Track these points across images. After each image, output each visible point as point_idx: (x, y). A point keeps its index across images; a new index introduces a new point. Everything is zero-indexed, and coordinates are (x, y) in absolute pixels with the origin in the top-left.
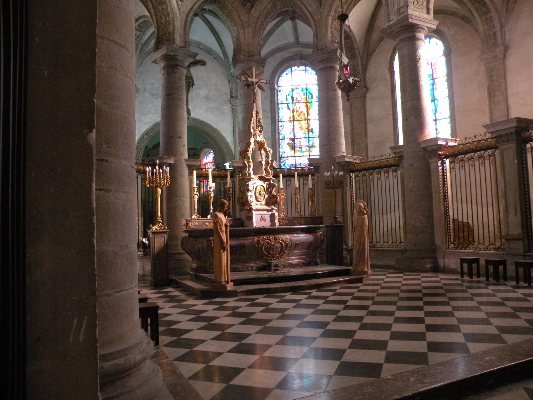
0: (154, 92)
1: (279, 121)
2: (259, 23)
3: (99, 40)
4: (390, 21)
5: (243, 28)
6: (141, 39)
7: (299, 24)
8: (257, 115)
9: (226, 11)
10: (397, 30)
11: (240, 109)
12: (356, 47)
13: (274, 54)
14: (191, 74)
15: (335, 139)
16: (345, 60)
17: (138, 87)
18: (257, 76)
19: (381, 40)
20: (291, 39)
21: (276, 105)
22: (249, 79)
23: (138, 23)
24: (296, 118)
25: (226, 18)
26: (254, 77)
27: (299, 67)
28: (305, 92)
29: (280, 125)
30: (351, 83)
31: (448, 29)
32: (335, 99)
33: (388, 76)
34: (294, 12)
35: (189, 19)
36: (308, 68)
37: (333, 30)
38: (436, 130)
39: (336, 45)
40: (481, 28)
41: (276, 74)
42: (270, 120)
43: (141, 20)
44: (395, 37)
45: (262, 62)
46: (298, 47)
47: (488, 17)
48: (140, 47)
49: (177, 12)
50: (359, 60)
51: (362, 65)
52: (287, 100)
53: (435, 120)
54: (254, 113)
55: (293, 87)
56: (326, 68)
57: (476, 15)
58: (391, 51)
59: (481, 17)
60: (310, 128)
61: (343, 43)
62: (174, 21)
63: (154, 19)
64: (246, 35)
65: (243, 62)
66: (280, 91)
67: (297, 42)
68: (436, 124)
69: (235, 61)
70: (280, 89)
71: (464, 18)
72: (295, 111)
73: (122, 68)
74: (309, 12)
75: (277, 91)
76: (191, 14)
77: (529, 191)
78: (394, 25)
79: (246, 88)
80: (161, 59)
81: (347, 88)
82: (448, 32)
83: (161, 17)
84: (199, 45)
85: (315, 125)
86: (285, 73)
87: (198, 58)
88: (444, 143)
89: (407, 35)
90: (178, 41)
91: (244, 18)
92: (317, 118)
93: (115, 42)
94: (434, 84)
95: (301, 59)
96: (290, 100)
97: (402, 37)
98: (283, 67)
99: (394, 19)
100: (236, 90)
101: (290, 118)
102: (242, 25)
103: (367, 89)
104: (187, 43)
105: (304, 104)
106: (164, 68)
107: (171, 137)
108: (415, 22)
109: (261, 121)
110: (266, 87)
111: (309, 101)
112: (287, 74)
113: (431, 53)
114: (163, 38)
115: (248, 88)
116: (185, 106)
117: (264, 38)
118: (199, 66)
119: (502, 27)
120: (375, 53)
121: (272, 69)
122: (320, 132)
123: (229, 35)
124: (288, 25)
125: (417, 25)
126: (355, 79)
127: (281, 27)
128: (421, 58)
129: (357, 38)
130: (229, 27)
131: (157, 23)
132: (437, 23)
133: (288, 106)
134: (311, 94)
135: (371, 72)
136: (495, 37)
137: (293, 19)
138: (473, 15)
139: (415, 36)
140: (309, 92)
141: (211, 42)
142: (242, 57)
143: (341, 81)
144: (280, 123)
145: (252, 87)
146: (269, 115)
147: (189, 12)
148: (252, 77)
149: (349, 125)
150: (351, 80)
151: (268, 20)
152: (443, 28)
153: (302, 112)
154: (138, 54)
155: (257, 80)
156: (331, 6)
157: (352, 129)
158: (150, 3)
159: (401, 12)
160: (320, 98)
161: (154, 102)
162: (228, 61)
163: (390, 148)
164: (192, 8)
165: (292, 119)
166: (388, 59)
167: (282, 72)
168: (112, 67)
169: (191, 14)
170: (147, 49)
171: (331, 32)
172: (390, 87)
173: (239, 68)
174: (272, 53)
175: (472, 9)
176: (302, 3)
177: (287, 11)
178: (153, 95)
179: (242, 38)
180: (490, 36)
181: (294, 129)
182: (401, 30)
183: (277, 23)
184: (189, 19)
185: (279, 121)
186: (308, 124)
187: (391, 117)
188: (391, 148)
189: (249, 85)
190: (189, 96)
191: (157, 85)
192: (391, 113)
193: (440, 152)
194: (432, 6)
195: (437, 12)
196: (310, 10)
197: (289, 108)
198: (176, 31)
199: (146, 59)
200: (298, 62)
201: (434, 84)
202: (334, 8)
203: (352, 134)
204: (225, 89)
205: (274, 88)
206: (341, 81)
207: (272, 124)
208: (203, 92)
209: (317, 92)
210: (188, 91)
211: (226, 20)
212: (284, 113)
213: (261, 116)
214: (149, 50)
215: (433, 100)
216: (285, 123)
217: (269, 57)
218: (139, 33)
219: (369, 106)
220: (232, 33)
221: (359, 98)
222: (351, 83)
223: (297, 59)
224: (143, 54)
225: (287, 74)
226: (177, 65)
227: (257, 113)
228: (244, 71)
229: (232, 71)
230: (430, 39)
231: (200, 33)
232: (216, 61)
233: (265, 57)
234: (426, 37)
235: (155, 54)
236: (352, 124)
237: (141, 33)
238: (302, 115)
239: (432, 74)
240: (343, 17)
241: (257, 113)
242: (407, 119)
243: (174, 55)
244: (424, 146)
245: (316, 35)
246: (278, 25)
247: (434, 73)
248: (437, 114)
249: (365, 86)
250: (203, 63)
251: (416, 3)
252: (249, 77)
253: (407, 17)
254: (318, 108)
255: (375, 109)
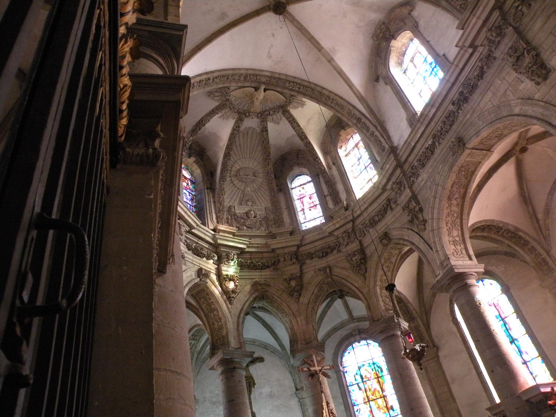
0: (214, 400)
1: (354, 405)
2: (310, 309)
3: (155, 372)
4: (437, 276)
5: (295, 318)
6: (196, 347)
7: (349, 300)
8: (328, 407)
9: (275, 304)
10: (447, 283)
11: (308, 402)
12: (412, 308)
13: (332, 335)
14: (250, 373)
15: (421, 413)
16: (405, 325)
17: (197, 398)
18: (319, 363)
19: (434, 295)
20: (345, 316)
21: (346, 388)
22: (312, 369)
23: (192, 333)
24: (371, 397)
25: (276, 312)
26: (316, 365)
27: (359, 342)
28: (373, 367)
29: (355, 410)
30: (419, 350)
31: (496, 267)
32: (408, 368)
33: (455, 329)
34: (341, 291)
35: (241, 320)
36: (369, 341)
37: (384, 298)
38: (532, 374)
39: (392, 312)
40: (528, 258)
41: (338, 355)
42: (343, 406)
43: (195, 329)
44: (447, 291)
45: (321, 347)
46: (354, 322)
47: (529, 247)
48: (196, 355)
49: (229, 315)
50: (419, 320)
51: (424, 325)
52: (356, 380)
53: (525, 363)
54: (324, 404)
55: (359, 365)
56: (387, 337)
57: (517, 248)
58: (449, 303)
59: (523, 250)
60: (389, 405)
61: (398, 308)
62: (226, 324)
63: (207, 326)
64: (300, 323)
65: (301, 351)
66: (346, 372)
67: (352, 318)
68: (528, 367)
69: (293, 351)
70: (346, 369)
71: (506, 254)
72: (368, 390)
73: (181, 397)
74: (356, 287)
75: (344, 373)
76: (242, 315)
77: (483, 187)
78: (442, 279)
79: (310, 378)
80: (218, 365)
81: (417, 357)
82: (498, 270)
83: (213, 324)
84: (253, 342)
85: (393, 400)
86: (347, 352)
87: (255, 355)
88: (548, 390)
89: (458, 286)
90: (233, 343)
91: (294, 307)
92: (394, 392)
93: (171, 371)
94: (505, 324)
95: (361, 334)
96: (359, 380)
97: (455, 287)
98: (344, 347)
99: (440, 273)
100: (300, 381)
101: (364, 399)
102: (294, 315)
103: (436, 348)
104: (242, 343)
105: (376, 380)
106: (222, 373)
107: (233, 400)
108: (461, 271)
109: (334, 411)
110: (330, 373)
111: (380, 375)
112: (349, 353)
113: (489, 294)
114: (218, 343)
115: (312, 378)
116: (250, 411)
117: (318, 321)
118: (258, 364)
119: (548, 253)
120: (433, 309)
121: (333, 351)
122: (400, 408)
123: (283, 327)
124: (338, 304)
125: (464, 273)
126: (422, 345)
127: (332, 307)
128: (481, 303)
129: (410, 300)
130: (281, 319)
131: (210, 330)
132: (483, 266)
133: (359, 386)
134: (379, 367)
135: (435, 329)
136: (547, 263)
137: (341, 297)
138: (514, 249)
139: (466, 283)
140: (377, 366)
141: (266, 337)
142: (299, 346)
143: (408, 351)
144: (355, 407)
145: (316, 376)
146: (341, 401)
147: (240, 313)
148: (314, 366)
149: (431, 393)
150: (417, 347)
151: (317, 304)
152: (491, 268)
153: (375, 389)
154: (194, 363)
155: (320, 368)
156: (375, 276)
157: (436, 396)
158: (202, 313)
159: (445, 265)
160: (391, 371)
161: (215, 411)
162: (286, 352)
163: (487, 409)
164: (242, 309)
165: (367, 400)
166: (448, 312)
167: (344, 351)
168: (170, 398)
169: (242, 315)
170: (203, 356)
171: (383, 301)
172: (460, 339)
173: (298, 358)
174: (329, 335)
175: (511, 244)
176: (347, 281)
177: (335, 291)
178: (214, 403)
179: (295, 327)
180: (541, 264)
181: (371, 411)
182: (452, 282)
183: (327, 305)
184: (241, 320)
185: (354, 405)
186: (386, 401)
187: (474, 371)
188: (489, 409)
189: (313, 375)
190: (252, 397)
191: (217, 392)
192: (472, 366)
193: (550, 402)
194: (471, 253)
195: (479, 256)
196: (357, 285)
197: (360, 389)
198: (229, 334)
199: (203, 366)
200: (358, 337)
201: (505, 324)
202: (378, 278)
203: (438, 403)
204: (288, 382)
205: (340, 371)
206: (408, 351)
207: (346, 410)
208: (266, 390)
209: (385, 363)
210: (250, 392)
211: (277, 314)
212: (357, 396)
213: (332, 405)
214: (205, 358)
215: (513, 341)
216: (360, 406)
217: (326, 340)
218: (193, 342)
219: (445, 366)
220: (284, 324)
221: (432, 359)
222: (419, 350)
223: (356, 335)
224: (199, 362)
225: (349, 353)
226: (235, 368)
227: (328, 403)
228: (304, 361)
229: (292, 363)
230: (482, 281)
231: (253, 330)
232: (274, 355)
233: (322, 340)
234: (478, 281)
235: (212, 359)
236: (433, 389)
237: (196, 342)
238: (377, 393)
239: (500, 315)
240: (391, 287)
241: (328, 403)
242: (492, 371)
243: (231, 358)
244: (526, 399)
245: (369, 307)
246: (328, 306)
247: (501, 313)
248: (523, 356)
249: (434, 346)
250: (261, 360)
251: (455, 254)
252: (310, 365)
253: (452, 269)
254: (391, 381)
255: (453, 367)
